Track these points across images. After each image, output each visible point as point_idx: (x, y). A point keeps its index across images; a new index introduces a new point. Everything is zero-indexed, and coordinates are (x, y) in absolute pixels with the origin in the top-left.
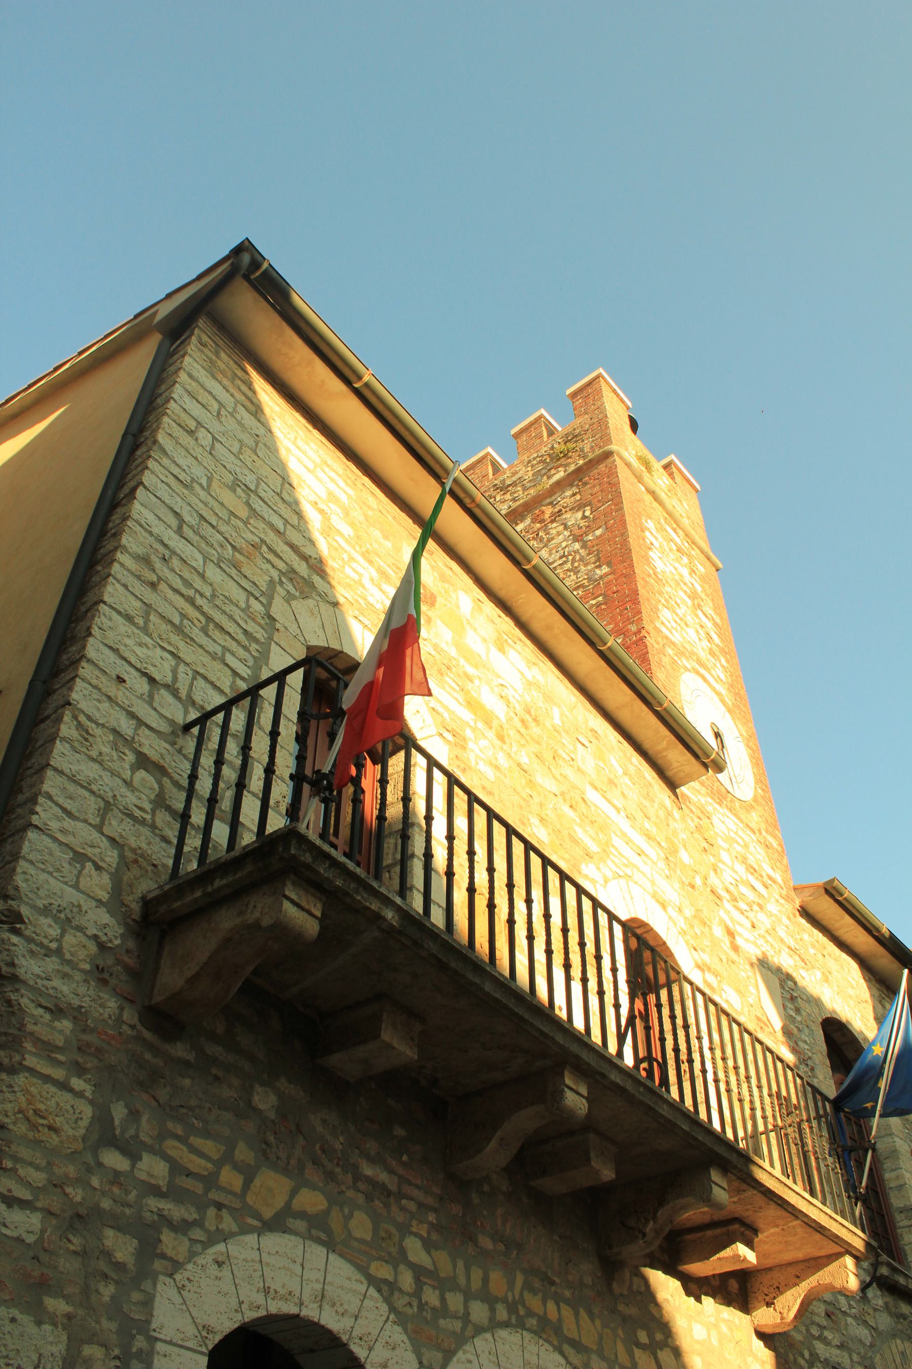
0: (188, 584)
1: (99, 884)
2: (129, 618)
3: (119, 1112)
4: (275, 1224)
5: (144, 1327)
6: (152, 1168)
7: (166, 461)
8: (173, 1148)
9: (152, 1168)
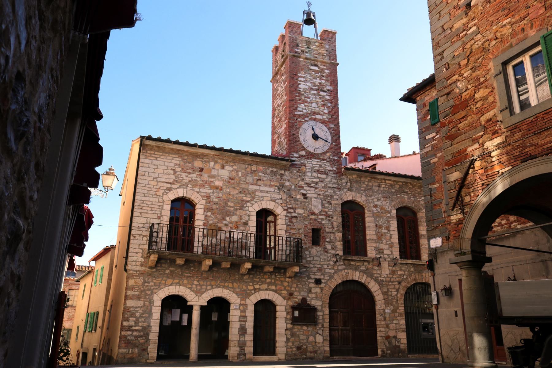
0: (147, 204)
1: (140, 255)
2: (138, 217)
3: (146, 279)
4: (171, 285)
5: (153, 299)
6: (152, 284)
7: (140, 185)
8: (154, 281)
9: (152, 284)
